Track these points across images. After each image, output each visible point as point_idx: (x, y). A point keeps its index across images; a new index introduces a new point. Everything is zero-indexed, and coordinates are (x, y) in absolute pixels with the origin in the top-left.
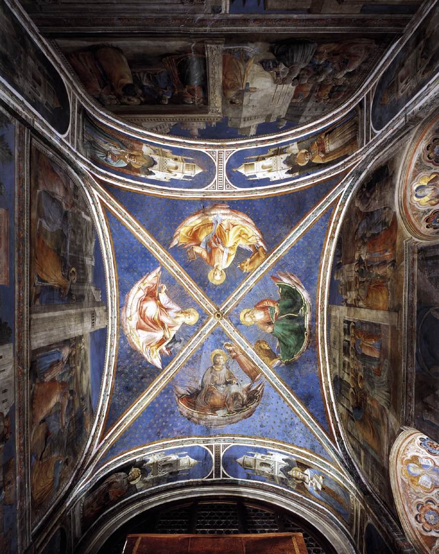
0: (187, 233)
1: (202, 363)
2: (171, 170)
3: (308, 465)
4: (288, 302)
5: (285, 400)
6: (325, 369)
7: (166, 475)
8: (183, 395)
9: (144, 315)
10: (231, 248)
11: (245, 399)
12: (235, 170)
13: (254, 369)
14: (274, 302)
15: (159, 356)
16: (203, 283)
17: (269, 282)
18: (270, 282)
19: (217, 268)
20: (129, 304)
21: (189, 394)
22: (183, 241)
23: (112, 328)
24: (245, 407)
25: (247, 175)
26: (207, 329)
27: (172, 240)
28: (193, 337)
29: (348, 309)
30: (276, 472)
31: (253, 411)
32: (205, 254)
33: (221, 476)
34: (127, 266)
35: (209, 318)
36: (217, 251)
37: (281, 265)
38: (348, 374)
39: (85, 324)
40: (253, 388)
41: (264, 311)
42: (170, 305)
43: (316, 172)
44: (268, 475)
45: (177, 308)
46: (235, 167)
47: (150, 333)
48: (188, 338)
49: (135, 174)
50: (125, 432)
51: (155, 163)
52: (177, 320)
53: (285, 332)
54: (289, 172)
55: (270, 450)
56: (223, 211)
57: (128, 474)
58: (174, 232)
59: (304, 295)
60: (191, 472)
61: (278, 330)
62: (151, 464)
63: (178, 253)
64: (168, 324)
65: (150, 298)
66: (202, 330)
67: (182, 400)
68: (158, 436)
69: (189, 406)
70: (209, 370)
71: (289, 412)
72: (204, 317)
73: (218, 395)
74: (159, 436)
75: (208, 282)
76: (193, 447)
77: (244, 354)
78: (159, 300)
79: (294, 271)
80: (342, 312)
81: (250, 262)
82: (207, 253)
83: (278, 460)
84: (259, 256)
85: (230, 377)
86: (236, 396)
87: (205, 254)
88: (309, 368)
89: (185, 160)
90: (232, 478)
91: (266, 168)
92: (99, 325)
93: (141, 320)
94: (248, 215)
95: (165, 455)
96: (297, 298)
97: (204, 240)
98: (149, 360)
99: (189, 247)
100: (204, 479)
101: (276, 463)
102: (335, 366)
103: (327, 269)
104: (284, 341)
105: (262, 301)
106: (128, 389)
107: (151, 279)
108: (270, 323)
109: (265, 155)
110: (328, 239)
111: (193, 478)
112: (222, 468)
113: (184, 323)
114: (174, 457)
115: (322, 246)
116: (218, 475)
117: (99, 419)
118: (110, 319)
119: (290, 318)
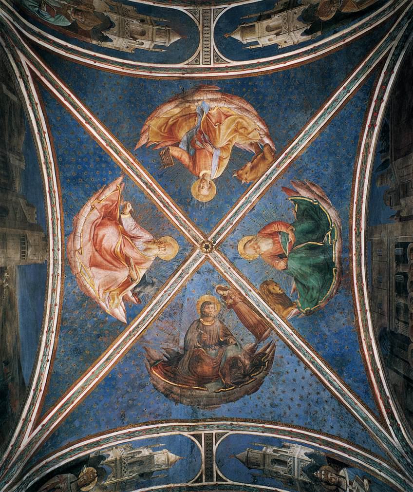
0: (160, 128)
1: (185, 315)
2: (136, 36)
3: (345, 462)
4: (306, 225)
5: (307, 367)
6: (365, 321)
7: (133, 477)
8: (158, 360)
9: (101, 246)
10: (223, 149)
11: (248, 367)
12: (227, 36)
13: (260, 322)
14: (287, 226)
15: (123, 303)
16: (184, 200)
17: (280, 197)
18: (282, 196)
19: (203, 179)
20: (79, 230)
21: (166, 359)
22: (154, 140)
23: (54, 264)
24: (247, 378)
25: (245, 42)
26: (192, 265)
27: (139, 136)
28: (171, 277)
29: (403, 225)
30: (296, 474)
31: (260, 383)
32: (186, 159)
33: (215, 479)
34: (74, 174)
35: (193, 250)
36: (204, 153)
37: (296, 170)
38: (406, 323)
39: (9, 251)
40: (260, 350)
41: (273, 238)
42: (137, 232)
43: (349, 26)
44: (283, 477)
45: (148, 237)
46: (226, 32)
47: (109, 272)
48: (164, 280)
49: (83, 38)
50: (71, 414)
51: (112, 25)
52: (148, 253)
53: (303, 268)
54: (306, 33)
55: (286, 440)
56: (210, 96)
57: (77, 476)
58: (142, 126)
59: (332, 214)
60: (171, 474)
61: (294, 265)
62: (112, 462)
63: (145, 155)
64: (134, 259)
65: (108, 222)
66: (183, 268)
67: (156, 367)
68: (123, 421)
69: (166, 376)
70: (195, 325)
71: (314, 385)
72: (186, 250)
73: (208, 361)
74: (123, 420)
75: (192, 198)
76: (174, 436)
77: (245, 301)
78: (122, 224)
79: (317, 178)
80: (391, 232)
81: (252, 168)
82: (190, 158)
83: (299, 453)
84: (264, 158)
85: (226, 335)
86: (234, 362)
87: (186, 159)
88: (340, 321)
89: (156, 22)
90: (230, 482)
91: (273, 31)
92: (32, 257)
93: (96, 254)
94: (248, 101)
95: (132, 448)
96: (320, 219)
97: (185, 138)
98: (108, 311)
99: (163, 149)
100: (189, 484)
101: (296, 460)
102: (382, 315)
103: (364, 175)
104: (304, 282)
105: (270, 225)
106: (77, 351)
107: (110, 193)
108: (281, 256)
109: (270, 12)
110: (367, 128)
111: (173, 483)
112: (215, 467)
113: (157, 258)
114: (146, 452)
115: (358, 139)
116: (209, 477)
117: (35, 394)
118: (51, 252)
119: (312, 248)
